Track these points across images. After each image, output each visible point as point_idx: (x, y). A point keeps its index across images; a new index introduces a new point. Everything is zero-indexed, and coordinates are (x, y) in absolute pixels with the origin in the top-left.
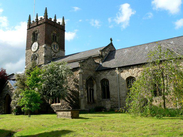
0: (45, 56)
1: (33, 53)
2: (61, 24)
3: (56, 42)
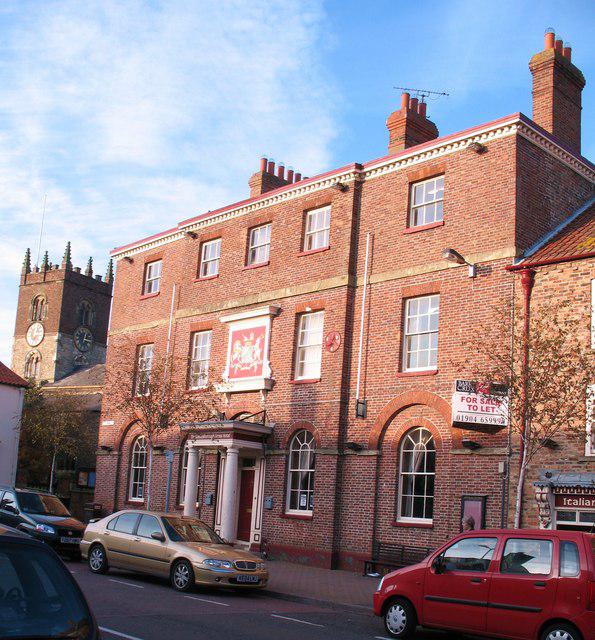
0: (57, 362)
1: (29, 349)
2: (103, 280)
3: (87, 326)
